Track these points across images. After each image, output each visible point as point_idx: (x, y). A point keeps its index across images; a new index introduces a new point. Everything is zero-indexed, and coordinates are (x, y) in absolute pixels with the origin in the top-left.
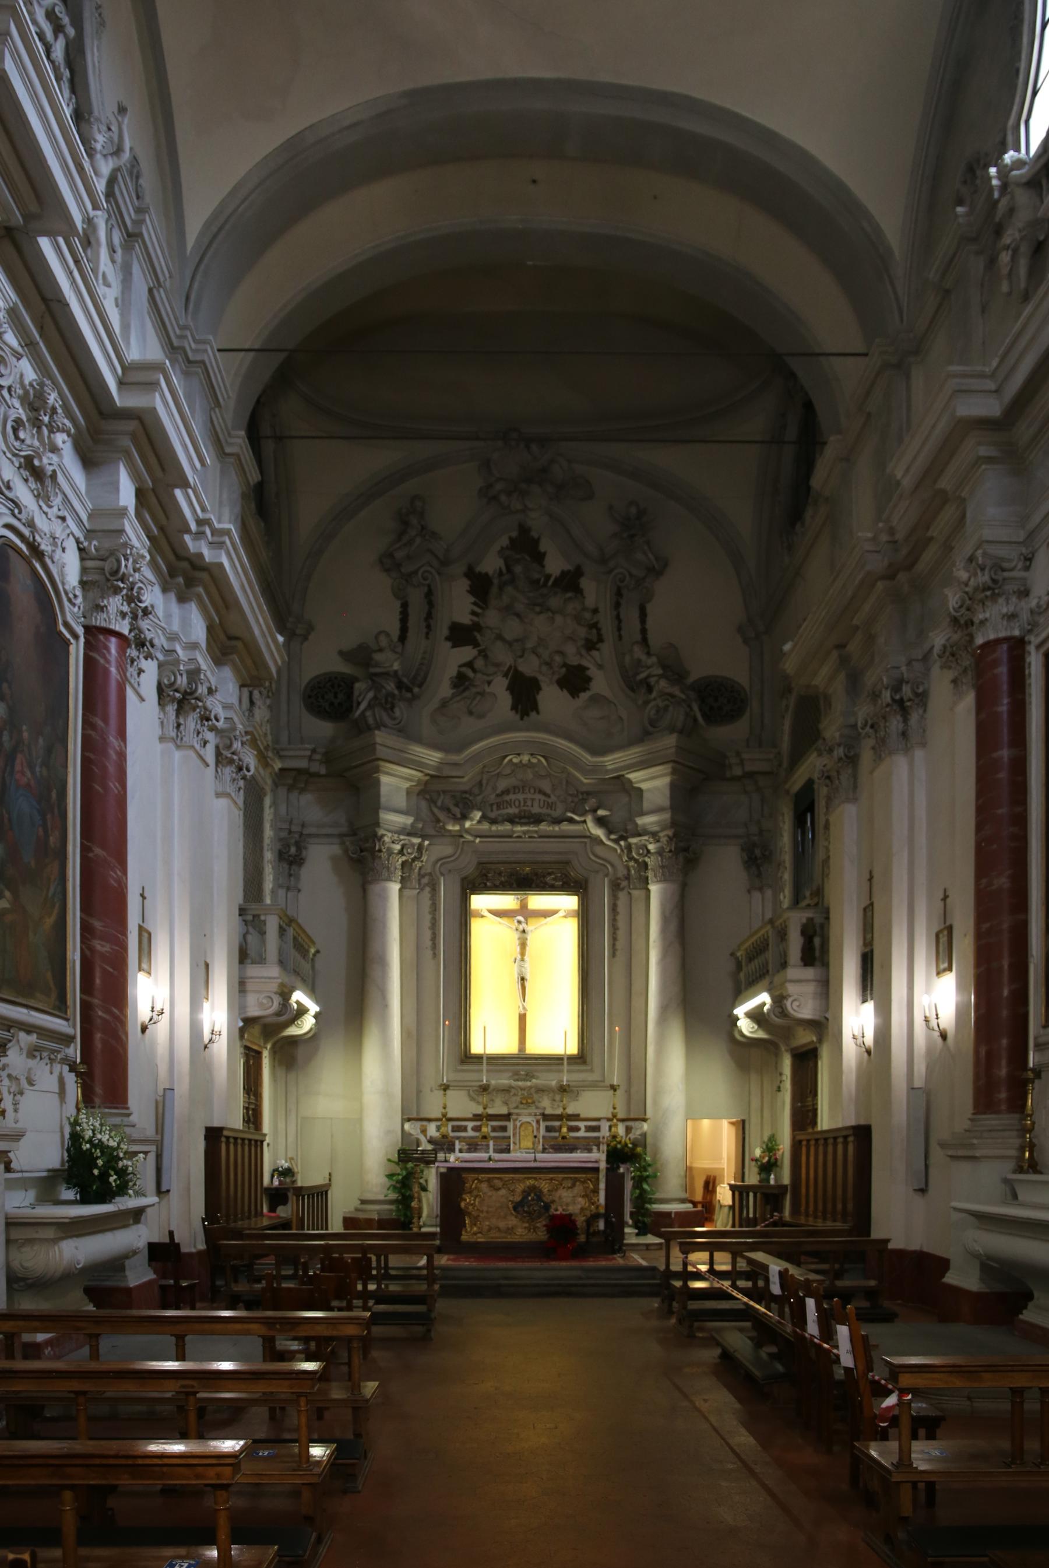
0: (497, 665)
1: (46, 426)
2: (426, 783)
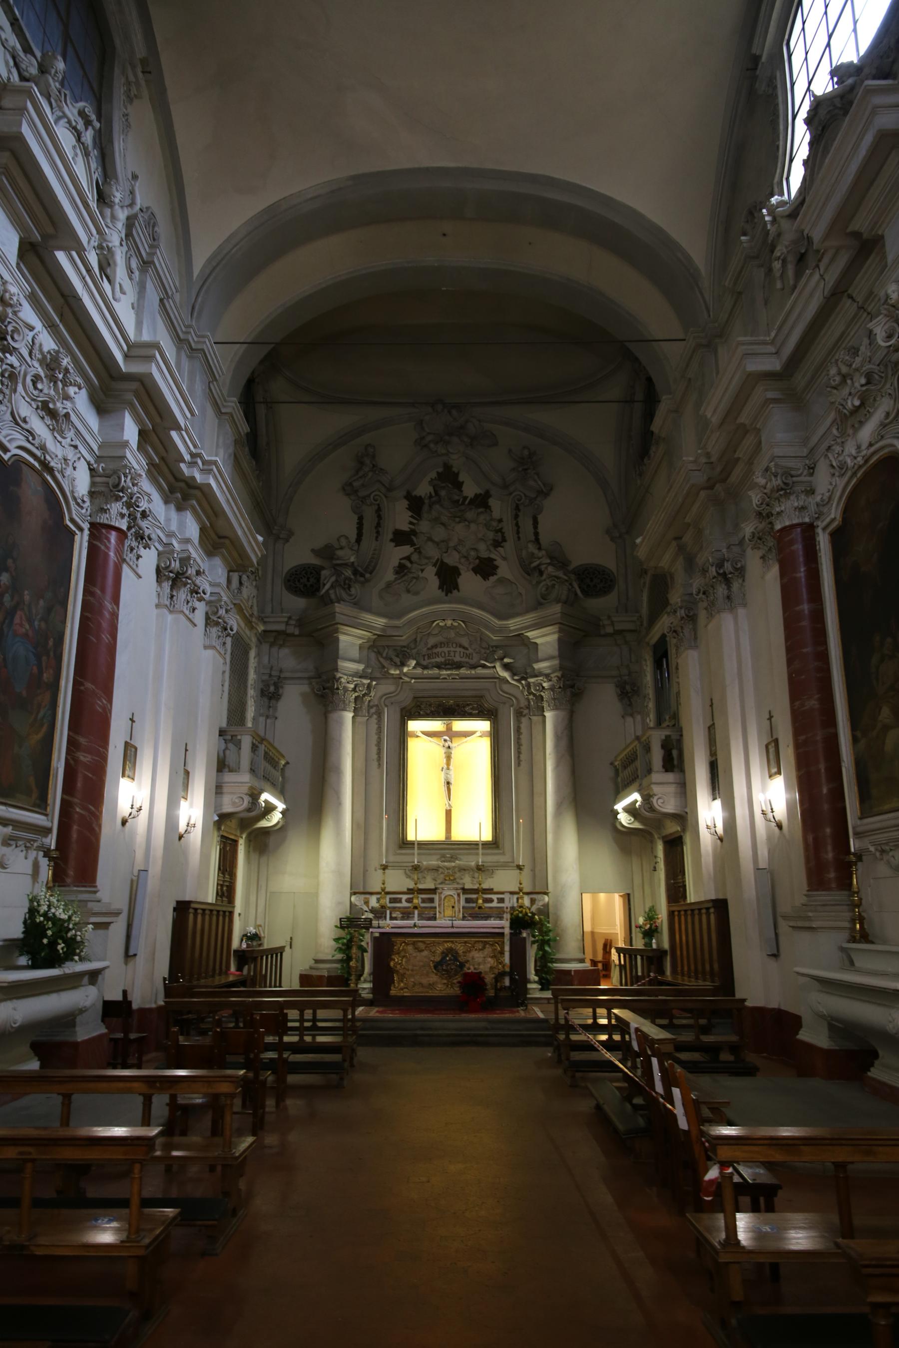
0: (428, 558)
1: (61, 381)
2: (375, 641)
